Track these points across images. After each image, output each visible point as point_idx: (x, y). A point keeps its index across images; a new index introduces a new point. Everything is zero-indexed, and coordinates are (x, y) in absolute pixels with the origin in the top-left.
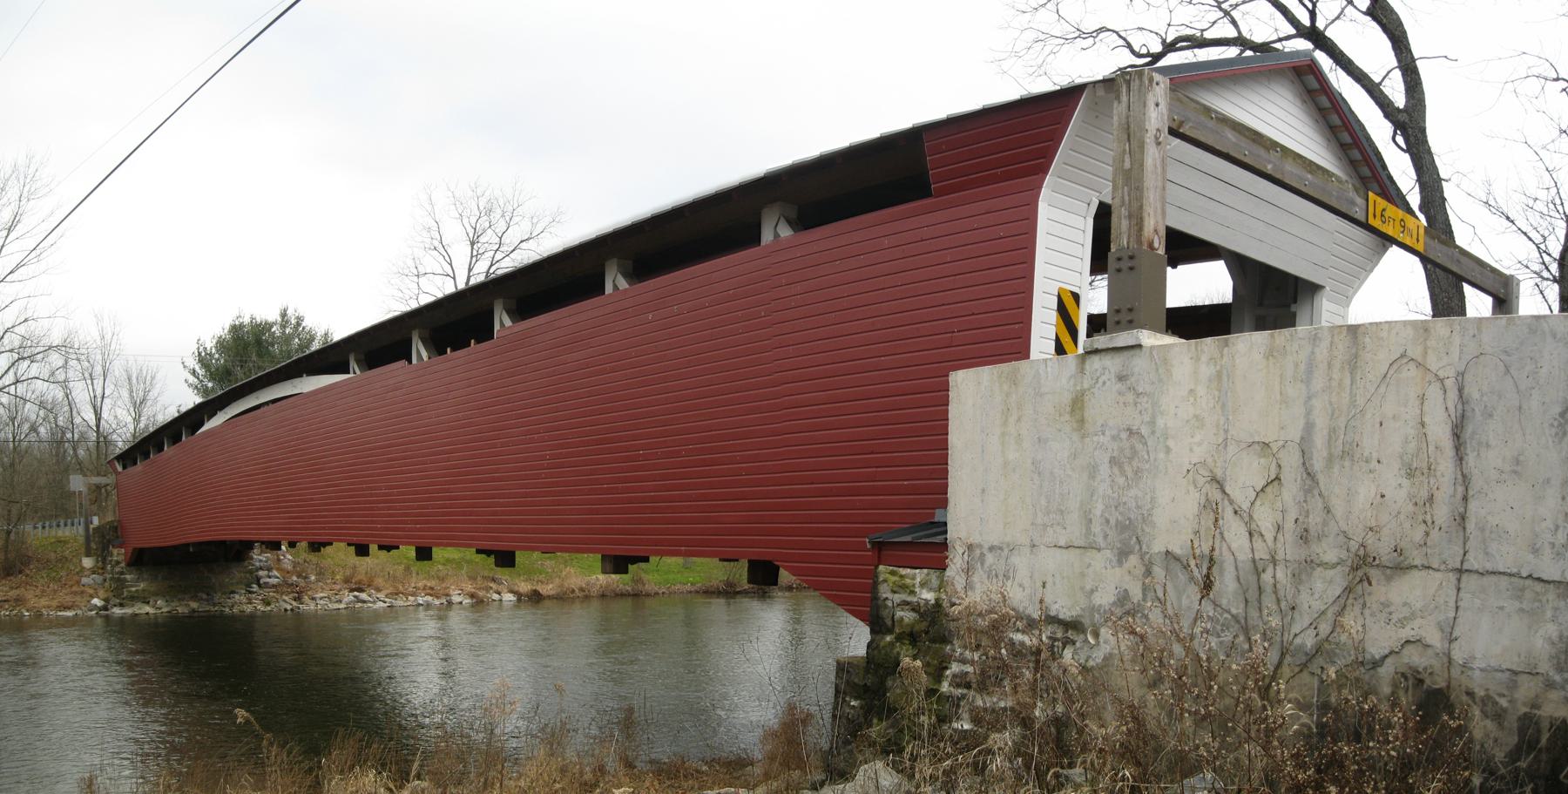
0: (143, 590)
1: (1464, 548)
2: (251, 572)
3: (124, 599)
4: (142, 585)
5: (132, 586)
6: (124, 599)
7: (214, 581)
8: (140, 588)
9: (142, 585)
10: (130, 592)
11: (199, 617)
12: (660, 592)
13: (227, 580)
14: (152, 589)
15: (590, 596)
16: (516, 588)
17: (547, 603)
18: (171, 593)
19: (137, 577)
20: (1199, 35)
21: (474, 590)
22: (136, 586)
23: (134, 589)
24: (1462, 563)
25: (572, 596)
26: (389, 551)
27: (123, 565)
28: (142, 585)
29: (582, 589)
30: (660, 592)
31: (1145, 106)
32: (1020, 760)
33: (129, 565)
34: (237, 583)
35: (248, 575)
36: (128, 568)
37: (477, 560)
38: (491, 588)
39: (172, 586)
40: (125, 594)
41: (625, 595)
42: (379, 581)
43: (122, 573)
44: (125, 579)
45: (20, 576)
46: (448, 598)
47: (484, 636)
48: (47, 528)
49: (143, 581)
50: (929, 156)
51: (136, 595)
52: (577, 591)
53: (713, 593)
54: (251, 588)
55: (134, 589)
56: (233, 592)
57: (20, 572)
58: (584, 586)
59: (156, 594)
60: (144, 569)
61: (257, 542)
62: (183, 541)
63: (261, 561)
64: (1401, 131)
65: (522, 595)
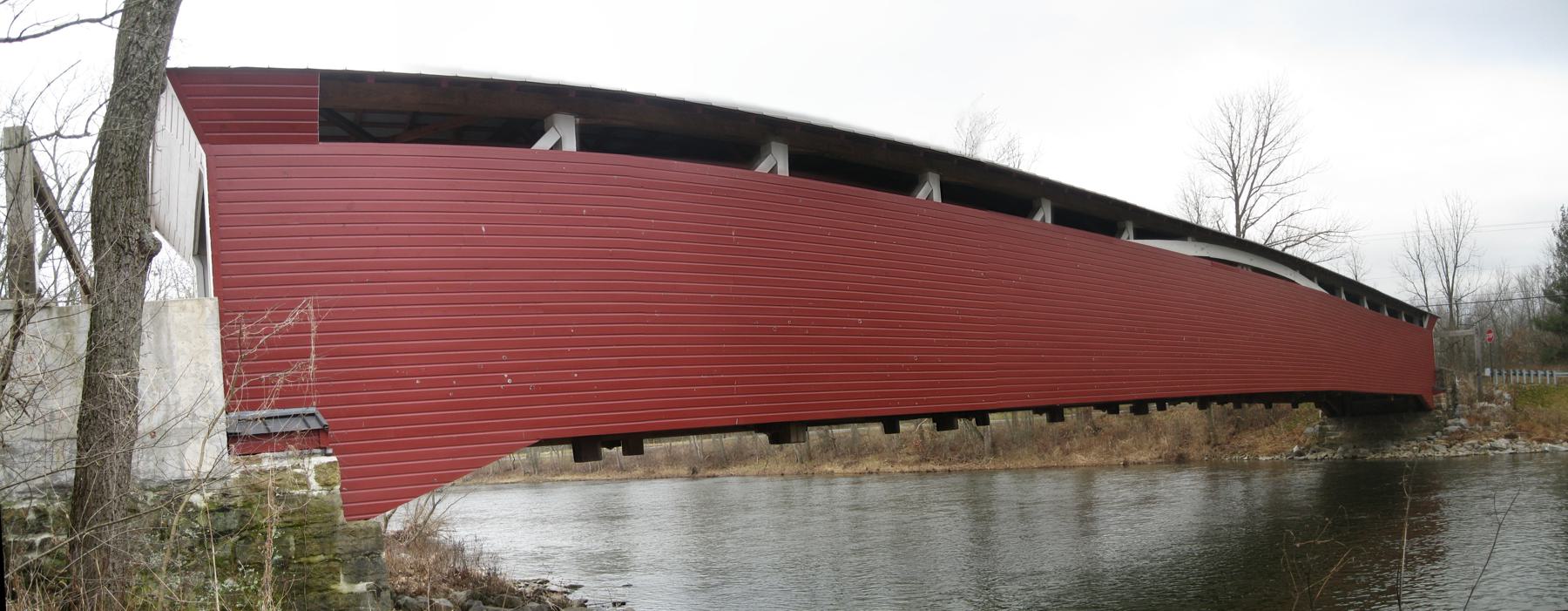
0: (1341, 438)
1: (53, 162)
4: (1340, 434)
5: (1331, 435)
7: (1403, 429)
10: (1330, 439)
13: (1416, 428)
14: (1349, 437)
20: (94, 165)
23: (1333, 437)
24: (72, 439)
26: (1295, 406)
28: (1340, 434)
31: (157, 105)
35: (1434, 423)
40: (1326, 441)
47: (658, 573)
50: (316, 112)
51: (1334, 442)
55: (1333, 437)
61: (1152, 401)
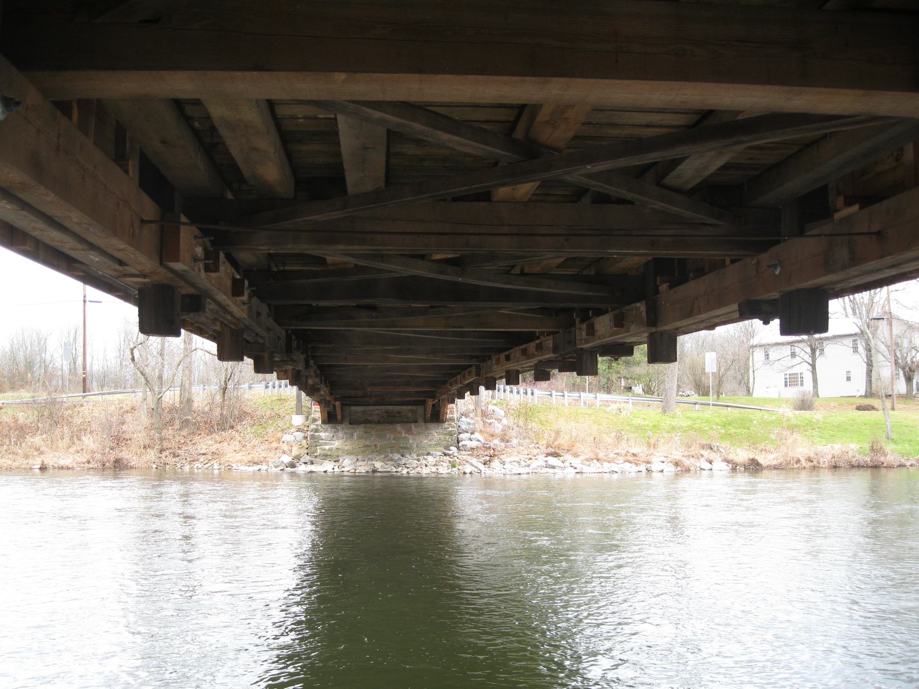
2: (451, 434)
3: (316, 457)
5: (326, 444)
6: (316, 457)
8: (334, 447)
9: (337, 444)
10: (325, 450)
11: (382, 477)
12: (908, 464)
14: (346, 448)
15: (819, 467)
16: (731, 457)
17: (765, 472)
18: (368, 451)
19: (331, 435)
21: (680, 458)
22: (331, 444)
23: (327, 447)
25: (796, 466)
27: (319, 422)
29: (810, 460)
30: (908, 464)
32: (321, 664)
33: (324, 422)
34: (436, 445)
36: (323, 426)
37: (706, 429)
38: (702, 456)
39: (367, 446)
40: (319, 452)
41: (863, 467)
42: (579, 447)
43: (316, 431)
44: (320, 438)
45: (230, 431)
46: (648, 465)
48: (270, 387)
49: (338, 439)
51: (329, 453)
52: (803, 461)
53: (863, 467)
54: (449, 450)
55: (327, 447)
56: (428, 454)
57: (232, 427)
58: (812, 455)
59: (349, 453)
60: (339, 428)
62: (704, 397)
63: (469, 424)
64: (187, 216)
65: (737, 465)
